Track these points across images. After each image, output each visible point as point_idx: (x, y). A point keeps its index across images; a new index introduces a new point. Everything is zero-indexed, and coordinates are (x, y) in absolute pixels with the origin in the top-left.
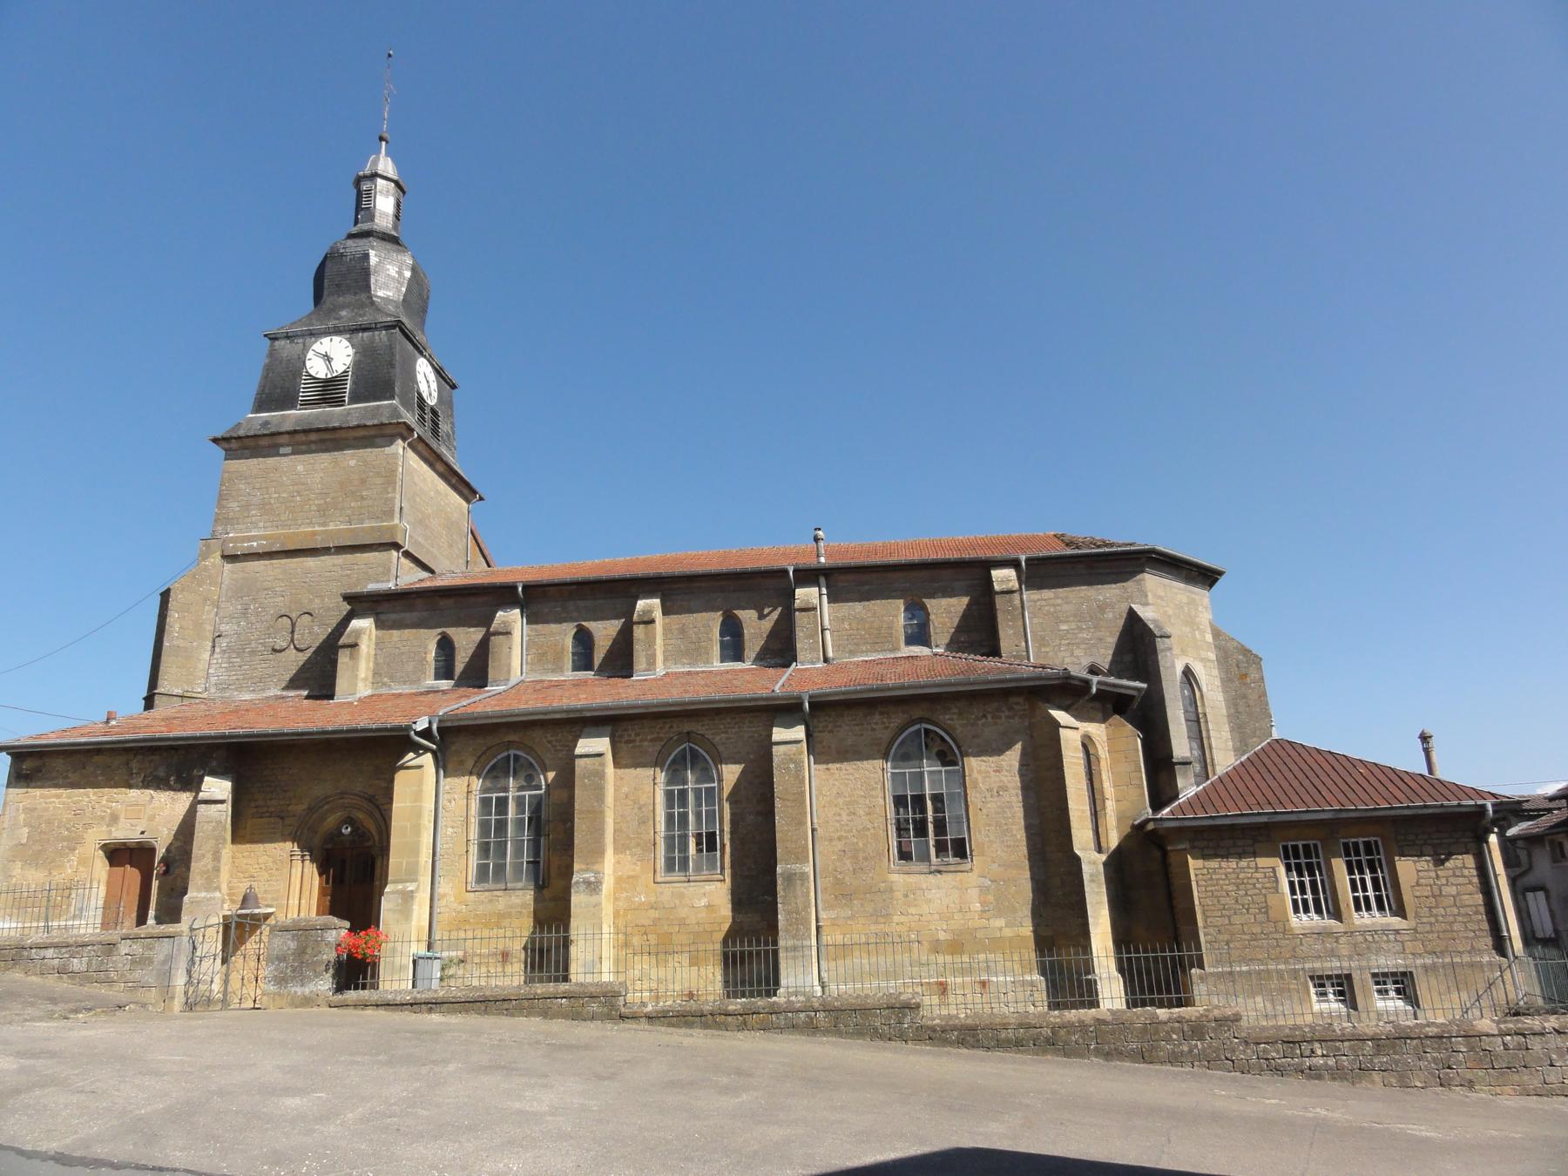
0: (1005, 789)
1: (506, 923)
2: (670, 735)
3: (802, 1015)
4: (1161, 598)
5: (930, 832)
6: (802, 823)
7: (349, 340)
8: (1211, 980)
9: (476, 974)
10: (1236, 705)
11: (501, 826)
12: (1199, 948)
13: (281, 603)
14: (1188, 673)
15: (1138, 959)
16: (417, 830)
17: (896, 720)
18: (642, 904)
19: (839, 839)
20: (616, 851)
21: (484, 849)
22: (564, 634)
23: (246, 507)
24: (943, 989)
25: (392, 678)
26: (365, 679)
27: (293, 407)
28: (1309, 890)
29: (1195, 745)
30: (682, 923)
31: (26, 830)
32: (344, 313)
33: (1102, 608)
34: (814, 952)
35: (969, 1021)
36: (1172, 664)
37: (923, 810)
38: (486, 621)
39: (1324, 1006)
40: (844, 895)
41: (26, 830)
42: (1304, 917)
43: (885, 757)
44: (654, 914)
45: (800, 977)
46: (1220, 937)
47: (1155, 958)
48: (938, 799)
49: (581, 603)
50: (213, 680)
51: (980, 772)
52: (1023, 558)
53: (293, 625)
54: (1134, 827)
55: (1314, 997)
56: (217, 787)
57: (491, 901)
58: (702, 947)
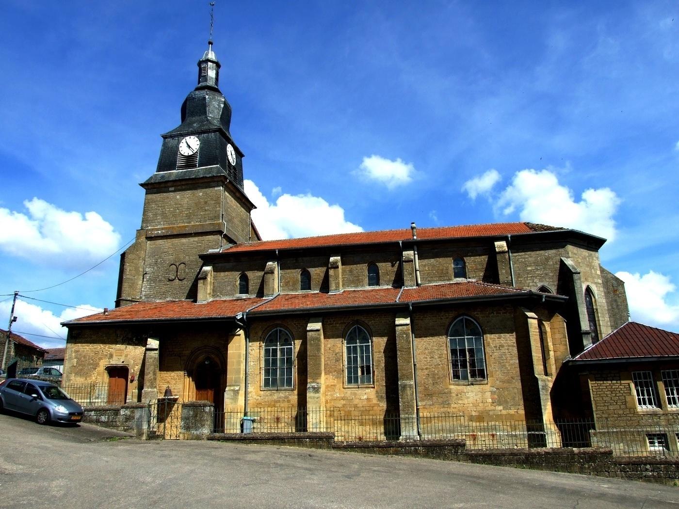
0: (503, 346)
1: (278, 405)
2: (352, 323)
3: (413, 448)
4: (576, 254)
5: (467, 366)
6: (409, 362)
7: (198, 137)
8: (598, 435)
9: (266, 427)
10: (612, 305)
11: (275, 362)
12: (593, 420)
13: (171, 258)
14: (588, 290)
15: (564, 425)
16: (239, 363)
17: (451, 315)
18: (337, 397)
19: (426, 369)
20: (326, 374)
21: (267, 372)
22: (297, 274)
23: (156, 215)
24: (474, 438)
25: (221, 293)
26: (210, 294)
27: (174, 169)
28: (646, 394)
29: (592, 324)
30: (356, 406)
31: (75, 360)
32: (195, 125)
33: (547, 259)
34: (415, 420)
35: (488, 452)
36: (581, 287)
37: (465, 356)
38: (262, 268)
39: (652, 449)
40: (429, 395)
41: (75, 360)
42: (644, 407)
43: (447, 334)
44: (343, 402)
45: (409, 432)
46: (604, 416)
47: (572, 425)
48: (471, 351)
49: (305, 259)
50: (144, 293)
51: (491, 338)
52: (510, 236)
53: (177, 269)
54: (564, 364)
55: (648, 444)
56: (153, 343)
57: (271, 395)
58: (364, 417)
